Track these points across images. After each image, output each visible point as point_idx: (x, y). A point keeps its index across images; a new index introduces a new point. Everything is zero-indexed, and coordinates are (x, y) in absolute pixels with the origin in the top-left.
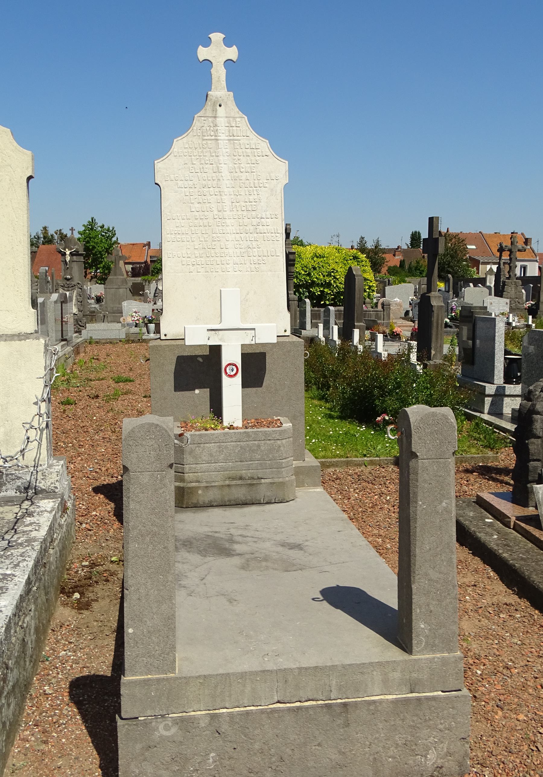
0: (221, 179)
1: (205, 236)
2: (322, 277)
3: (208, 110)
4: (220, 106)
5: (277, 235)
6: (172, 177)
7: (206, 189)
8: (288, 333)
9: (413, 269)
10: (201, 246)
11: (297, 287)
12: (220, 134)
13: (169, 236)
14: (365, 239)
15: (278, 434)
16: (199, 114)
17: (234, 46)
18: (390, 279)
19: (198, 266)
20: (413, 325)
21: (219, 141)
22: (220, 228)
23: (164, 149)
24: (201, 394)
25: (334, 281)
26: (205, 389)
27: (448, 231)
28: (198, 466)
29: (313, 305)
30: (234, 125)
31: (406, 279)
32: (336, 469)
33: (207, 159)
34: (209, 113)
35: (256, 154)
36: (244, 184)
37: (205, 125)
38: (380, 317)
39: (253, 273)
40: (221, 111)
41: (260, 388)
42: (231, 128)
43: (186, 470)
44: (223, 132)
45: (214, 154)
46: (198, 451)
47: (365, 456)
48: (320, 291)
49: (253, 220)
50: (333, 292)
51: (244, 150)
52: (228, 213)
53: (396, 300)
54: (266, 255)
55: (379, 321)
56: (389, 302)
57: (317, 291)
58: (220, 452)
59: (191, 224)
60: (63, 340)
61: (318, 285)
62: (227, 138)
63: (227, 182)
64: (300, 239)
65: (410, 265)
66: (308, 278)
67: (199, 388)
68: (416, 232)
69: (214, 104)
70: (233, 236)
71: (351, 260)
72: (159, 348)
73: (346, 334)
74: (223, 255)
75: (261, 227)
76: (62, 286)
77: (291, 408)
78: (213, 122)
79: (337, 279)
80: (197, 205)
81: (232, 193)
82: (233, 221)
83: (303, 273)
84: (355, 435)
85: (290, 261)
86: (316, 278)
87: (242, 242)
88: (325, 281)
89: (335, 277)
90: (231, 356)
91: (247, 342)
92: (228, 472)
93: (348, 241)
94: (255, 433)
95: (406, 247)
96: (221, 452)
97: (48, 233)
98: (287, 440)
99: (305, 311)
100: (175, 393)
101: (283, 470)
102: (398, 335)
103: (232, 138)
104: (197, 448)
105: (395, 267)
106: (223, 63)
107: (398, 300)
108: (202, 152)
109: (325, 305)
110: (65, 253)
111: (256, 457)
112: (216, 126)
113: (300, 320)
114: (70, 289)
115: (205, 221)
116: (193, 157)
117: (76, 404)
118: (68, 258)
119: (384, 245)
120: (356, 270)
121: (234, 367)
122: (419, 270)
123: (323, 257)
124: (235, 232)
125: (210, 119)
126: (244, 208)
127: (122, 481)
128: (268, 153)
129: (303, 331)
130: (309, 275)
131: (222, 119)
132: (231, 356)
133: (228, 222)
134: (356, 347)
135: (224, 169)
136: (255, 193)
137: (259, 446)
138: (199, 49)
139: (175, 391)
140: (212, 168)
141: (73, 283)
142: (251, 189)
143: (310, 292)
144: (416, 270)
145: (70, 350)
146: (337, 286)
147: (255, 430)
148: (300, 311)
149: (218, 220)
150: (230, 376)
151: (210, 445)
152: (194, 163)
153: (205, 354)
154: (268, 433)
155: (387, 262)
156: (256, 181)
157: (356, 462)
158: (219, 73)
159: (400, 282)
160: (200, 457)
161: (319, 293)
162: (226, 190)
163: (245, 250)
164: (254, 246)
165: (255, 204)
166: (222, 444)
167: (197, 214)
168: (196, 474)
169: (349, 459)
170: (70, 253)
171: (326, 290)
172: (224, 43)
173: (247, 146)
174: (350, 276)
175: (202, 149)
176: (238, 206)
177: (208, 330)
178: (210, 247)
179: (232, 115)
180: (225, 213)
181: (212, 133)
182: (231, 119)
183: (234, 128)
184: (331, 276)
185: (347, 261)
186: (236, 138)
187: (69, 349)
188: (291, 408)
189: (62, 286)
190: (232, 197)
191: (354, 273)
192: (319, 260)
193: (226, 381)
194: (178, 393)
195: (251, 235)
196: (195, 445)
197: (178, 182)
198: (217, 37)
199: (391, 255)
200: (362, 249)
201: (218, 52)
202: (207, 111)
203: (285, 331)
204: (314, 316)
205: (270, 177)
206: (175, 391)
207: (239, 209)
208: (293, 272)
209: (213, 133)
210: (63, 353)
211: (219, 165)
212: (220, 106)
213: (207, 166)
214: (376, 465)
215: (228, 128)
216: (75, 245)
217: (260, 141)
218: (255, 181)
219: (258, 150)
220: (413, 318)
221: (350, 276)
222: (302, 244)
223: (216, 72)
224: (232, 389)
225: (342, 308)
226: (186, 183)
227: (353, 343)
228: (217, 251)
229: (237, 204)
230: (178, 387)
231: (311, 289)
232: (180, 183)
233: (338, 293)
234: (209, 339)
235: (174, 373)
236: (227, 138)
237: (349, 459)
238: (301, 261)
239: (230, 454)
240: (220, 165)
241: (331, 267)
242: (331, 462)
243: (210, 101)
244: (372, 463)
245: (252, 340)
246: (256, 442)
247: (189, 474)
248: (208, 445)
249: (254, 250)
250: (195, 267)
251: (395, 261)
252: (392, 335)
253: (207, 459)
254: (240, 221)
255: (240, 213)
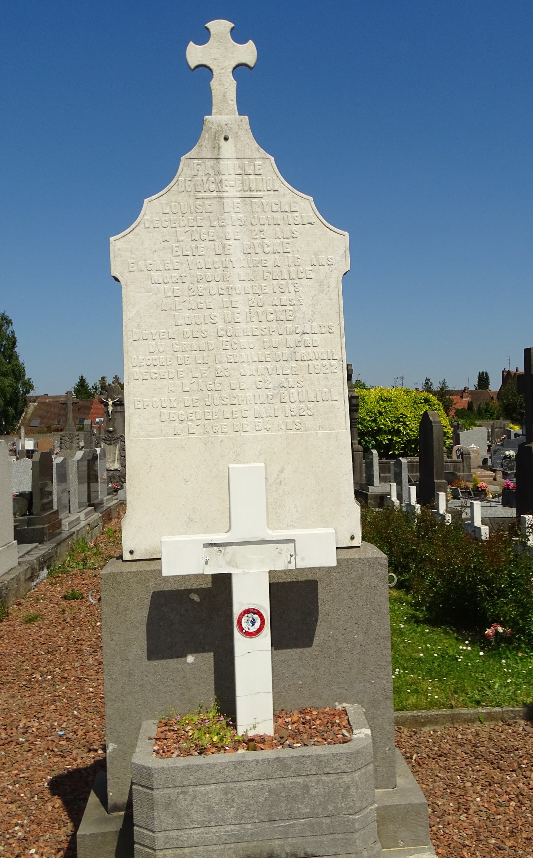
0: (230, 265)
1: (203, 368)
2: (389, 423)
3: (203, 147)
4: (226, 139)
5: (333, 362)
6: (141, 263)
7: (203, 285)
8: (358, 541)
9: (483, 411)
10: (195, 386)
11: (362, 435)
12: (227, 188)
13: (136, 369)
14: (430, 381)
15: (344, 761)
16: (188, 155)
17: (250, 41)
18: (460, 423)
19: (190, 423)
20: (494, 474)
21: (225, 200)
22: (230, 353)
23: (126, 216)
24: (197, 664)
25: (403, 428)
26: (206, 654)
27: (517, 371)
28: (182, 833)
29: (381, 456)
30: (250, 172)
31: (476, 422)
32: (436, 727)
33: (204, 231)
34: (207, 152)
35: (291, 221)
36: (271, 273)
37: (200, 173)
38: (459, 469)
39: (290, 432)
40: (228, 149)
41: (309, 650)
42: (246, 177)
43: (160, 844)
44: (232, 183)
45: (216, 223)
46: (183, 802)
47: (478, 703)
48: (388, 439)
49: (288, 337)
50: (402, 440)
51: (269, 214)
52: (243, 325)
53: (472, 446)
54: (314, 399)
55: (458, 474)
56: (468, 452)
57: (384, 439)
58: (227, 802)
59: (176, 347)
60: (89, 506)
61: (385, 432)
62: (239, 194)
63: (241, 271)
64: (362, 383)
65: (479, 407)
66: (374, 424)
67: (195, 651)
68: (483, 373)
69: (215, 138)
70: (253, 366)
71: (421, 403)
72: (119, 579)
73: (427, 497)
74: (235, 402)
75: (302, 350)
76: (104, 440)
77: (368, 685)
78: (213, 168)
79: (407, 425)
80: (187, 314)
81: (250, 291)
82: (252, 339)
83: (368, 418)
84: (457, 659)
85: (354, 408)
86: (383, 424)
87: (269, 378)
88: (394, 428)
89: (404, 423)
90: (251, 594)
91: (281, 565)
92: (244, 845)
93: (414, 382)
94: (298, 760)
95: (474, 389)
96: (229, 802)
97: (105, 383)
98: (363, 770)
99: (372, 463)
100: (148, 663)
101: (356, 836)
102: (484, 490)
103: (247, 194)
104: (181, 797)
105: (463, 409)
106: (231, 70)
107: (475, 446)
108: (195, 219)
109: (394, 456)
110: (108, 403)
111: (302, 811)
112: (219, 173)
113: (366, 473)
114: (112, 442)
115: (202, 341)
116: (178, 229)
117: (83, 598)
118: (111, 409)
119: (450, 386)
120: (432, 416)
121: (256, 617)
122: (489, 412)
123: (391, 401)
124: (256, 359)
125: (209, 163)
126: (271, 317)
127: (105, 759)
128: (314, 219)
129: (370, 487)
130: (375, 421)
131: (230, 162)
132: (251, 594)
133: (243, 341)
134: (443, 516)
135: (236, 249)
136: (292, 288)
137: (306, 788)
138: (189, 47)
139: (149, 659)
140: (212, 247)
141: (116, 436)
142: (283, 282)
143: (376, 440)
144: (485, 412)
145: (97, 518)
146: (407, 433)
147: (299, 751)
148: (366, 463)
149: (225, 338)
150: (249, 634)
151: (208, 788)
152: (182, 238)
153: (203, 586)
154: (325, 759)
155: (455, 404)
156: (293, 269)
157: (466, 717)
158: (224, 88)
159: (470, 425)
160: (188, 815)
161: (387, 442)
162: (238, 285)
163: (276, 391)
164: (292, 384)
165: (291, 308)
166: (232, 785)
167: (187, 329)
168: (179, 851)
169: (456, 711)
170: (113, 403)
171: (395, 438)
172: (231, 36)
173: (275, 208)
174: (426, 423)
175: (195, 214)
176: (260, 313)
177: (205, 545)
178: (212, 387)
179: (248, 154)
180: (237, 326)
181: (213, 187)
182: (246, 162)
183: (250, 177)
184: (400, 422)
185: (417, 404)
186: (255, 194)
187: (97, 516)
188: (368, 685)
189: (104, 440)
190: (250, 296)
191: (431, 419)
192: (386, 404)
193: (240, 642)
194: (155, 663)
195: (286, 364)
196: (178, 790)
197: (152, 273)
198: (220, 27)
199: (458, 397)
200: (428, 388)
201: (222, 52)
202: (203, 148)
203: (352, 538)
204: (383, 469)
205: (318, 260)
206: (149, 659)
207: (263, 318)
208: (356, 419)
209: (214, 186)
210: (87, 522)
211: (224, 241)
212: (226, 139)
213: (203, 244)
214: (497, 721)
215: (240, 177)
216: (119, 395)
217: (298, 199)
218: (291, 269)
219: (295, 214)
220: (493, 466)
221: (426, 423)
222: (363, 387)
223: (220, 85)
224: (254, 659)
225: (416, 459)
226: (166, 274)
227: (438, 511)
228: (224, 394)
229: (260, 310)
230: (155, 652)
231: (378, 438)
232: (156, 276)
233: (409, 441)
234: (207, 563)
235: (148, 625)
236: (239, 194)
237: (456, 711)
238: (366, 406)
239: (248, 806)
240: (228, 242)
241: (399, 412)
242: (426, 717)
243: (207, 131)
244: (490, 717)
245: (290, 562)
246: (300, 780)
247: (166, 852)
248: (202, 788)
249: (292, 390)
250: (184, 424)
251: (463, 403)
252: (476, 491)
253: (201, 819)
254: (266, 339)
255: (264, 325)
